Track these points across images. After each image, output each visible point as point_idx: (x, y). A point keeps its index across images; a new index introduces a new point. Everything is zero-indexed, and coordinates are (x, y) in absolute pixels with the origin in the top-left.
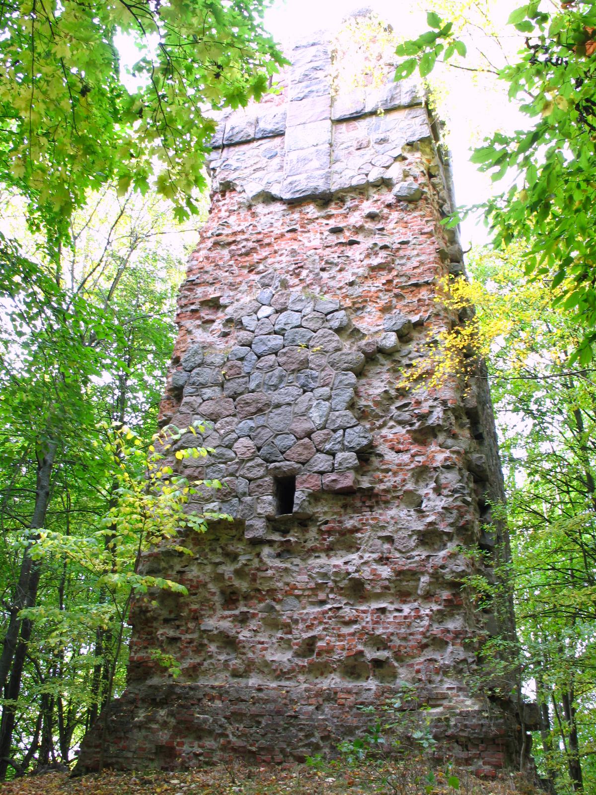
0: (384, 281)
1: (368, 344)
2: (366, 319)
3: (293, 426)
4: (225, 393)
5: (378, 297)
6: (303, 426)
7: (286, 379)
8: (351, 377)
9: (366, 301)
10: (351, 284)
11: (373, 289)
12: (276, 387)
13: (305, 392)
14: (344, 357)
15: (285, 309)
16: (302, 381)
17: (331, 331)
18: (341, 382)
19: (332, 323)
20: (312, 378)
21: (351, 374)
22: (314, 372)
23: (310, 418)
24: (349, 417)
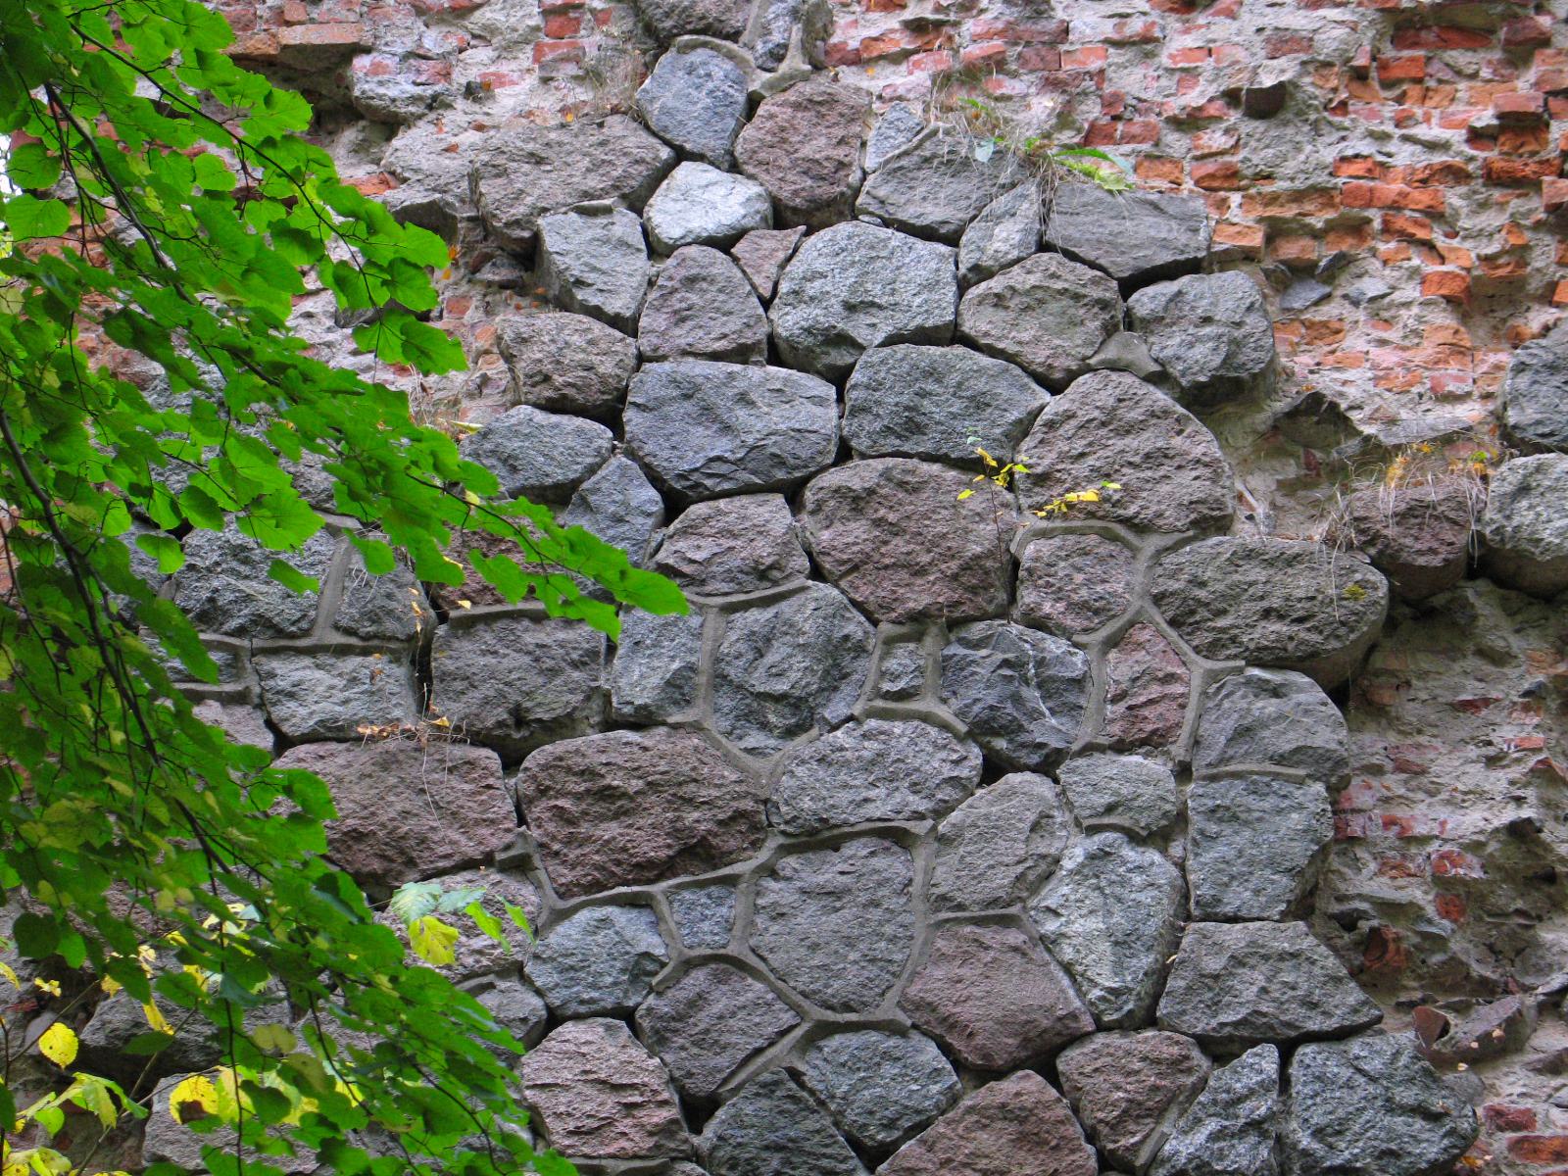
0: (1485, 117)
1: (1412, 514)
2: (1354, 343)
3: (934, 983)
4: (448, 712)
5: (1435, 214)
6: (997, 993)
7: (868, 666)
8: (1307, 713)
9: (1357, 229)
10: (1268, 104)
11: (1405, 156)
12: (800, 714)
13: (993, 769)
14: (1255, 573)
15: (843, 208)
16: (982, 693)
17: (1160, 397)
18: (1244, 732)
19: (1169, 344)
20: (1048, 687)
21: (1307, 692)
22: (1055, 646)
23: (1049, 943)
24: (1308, 974)
